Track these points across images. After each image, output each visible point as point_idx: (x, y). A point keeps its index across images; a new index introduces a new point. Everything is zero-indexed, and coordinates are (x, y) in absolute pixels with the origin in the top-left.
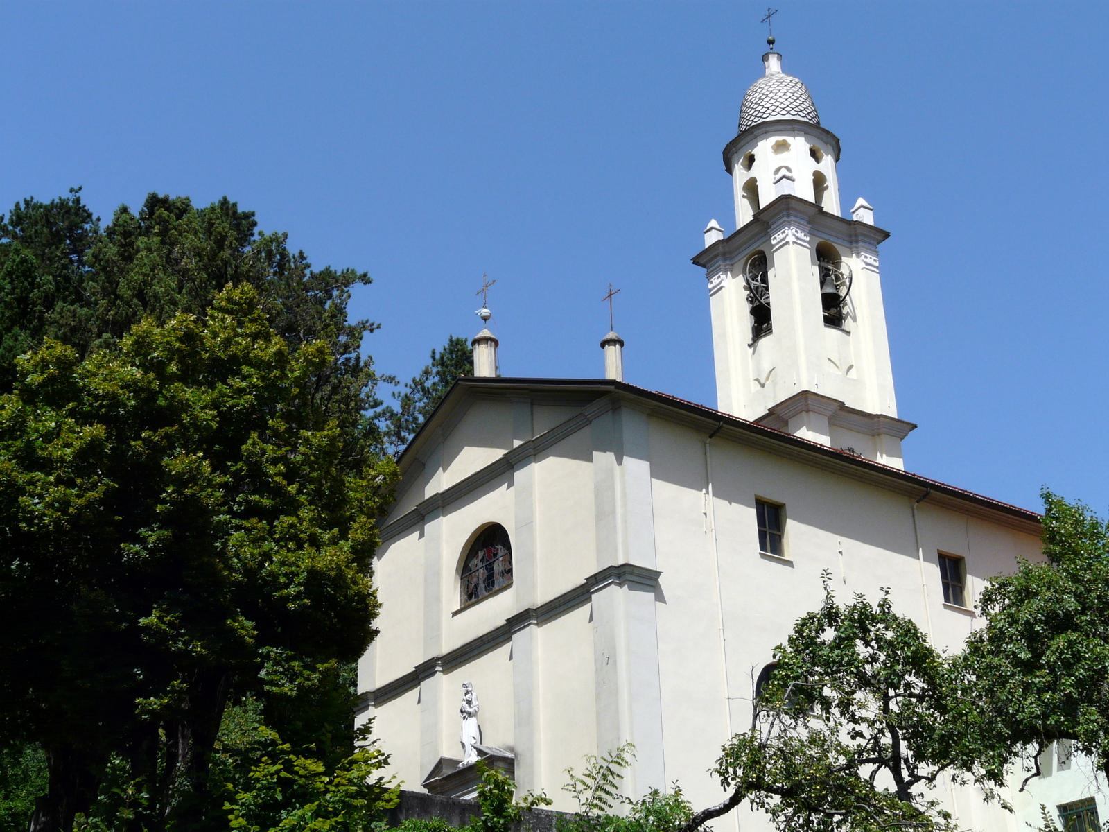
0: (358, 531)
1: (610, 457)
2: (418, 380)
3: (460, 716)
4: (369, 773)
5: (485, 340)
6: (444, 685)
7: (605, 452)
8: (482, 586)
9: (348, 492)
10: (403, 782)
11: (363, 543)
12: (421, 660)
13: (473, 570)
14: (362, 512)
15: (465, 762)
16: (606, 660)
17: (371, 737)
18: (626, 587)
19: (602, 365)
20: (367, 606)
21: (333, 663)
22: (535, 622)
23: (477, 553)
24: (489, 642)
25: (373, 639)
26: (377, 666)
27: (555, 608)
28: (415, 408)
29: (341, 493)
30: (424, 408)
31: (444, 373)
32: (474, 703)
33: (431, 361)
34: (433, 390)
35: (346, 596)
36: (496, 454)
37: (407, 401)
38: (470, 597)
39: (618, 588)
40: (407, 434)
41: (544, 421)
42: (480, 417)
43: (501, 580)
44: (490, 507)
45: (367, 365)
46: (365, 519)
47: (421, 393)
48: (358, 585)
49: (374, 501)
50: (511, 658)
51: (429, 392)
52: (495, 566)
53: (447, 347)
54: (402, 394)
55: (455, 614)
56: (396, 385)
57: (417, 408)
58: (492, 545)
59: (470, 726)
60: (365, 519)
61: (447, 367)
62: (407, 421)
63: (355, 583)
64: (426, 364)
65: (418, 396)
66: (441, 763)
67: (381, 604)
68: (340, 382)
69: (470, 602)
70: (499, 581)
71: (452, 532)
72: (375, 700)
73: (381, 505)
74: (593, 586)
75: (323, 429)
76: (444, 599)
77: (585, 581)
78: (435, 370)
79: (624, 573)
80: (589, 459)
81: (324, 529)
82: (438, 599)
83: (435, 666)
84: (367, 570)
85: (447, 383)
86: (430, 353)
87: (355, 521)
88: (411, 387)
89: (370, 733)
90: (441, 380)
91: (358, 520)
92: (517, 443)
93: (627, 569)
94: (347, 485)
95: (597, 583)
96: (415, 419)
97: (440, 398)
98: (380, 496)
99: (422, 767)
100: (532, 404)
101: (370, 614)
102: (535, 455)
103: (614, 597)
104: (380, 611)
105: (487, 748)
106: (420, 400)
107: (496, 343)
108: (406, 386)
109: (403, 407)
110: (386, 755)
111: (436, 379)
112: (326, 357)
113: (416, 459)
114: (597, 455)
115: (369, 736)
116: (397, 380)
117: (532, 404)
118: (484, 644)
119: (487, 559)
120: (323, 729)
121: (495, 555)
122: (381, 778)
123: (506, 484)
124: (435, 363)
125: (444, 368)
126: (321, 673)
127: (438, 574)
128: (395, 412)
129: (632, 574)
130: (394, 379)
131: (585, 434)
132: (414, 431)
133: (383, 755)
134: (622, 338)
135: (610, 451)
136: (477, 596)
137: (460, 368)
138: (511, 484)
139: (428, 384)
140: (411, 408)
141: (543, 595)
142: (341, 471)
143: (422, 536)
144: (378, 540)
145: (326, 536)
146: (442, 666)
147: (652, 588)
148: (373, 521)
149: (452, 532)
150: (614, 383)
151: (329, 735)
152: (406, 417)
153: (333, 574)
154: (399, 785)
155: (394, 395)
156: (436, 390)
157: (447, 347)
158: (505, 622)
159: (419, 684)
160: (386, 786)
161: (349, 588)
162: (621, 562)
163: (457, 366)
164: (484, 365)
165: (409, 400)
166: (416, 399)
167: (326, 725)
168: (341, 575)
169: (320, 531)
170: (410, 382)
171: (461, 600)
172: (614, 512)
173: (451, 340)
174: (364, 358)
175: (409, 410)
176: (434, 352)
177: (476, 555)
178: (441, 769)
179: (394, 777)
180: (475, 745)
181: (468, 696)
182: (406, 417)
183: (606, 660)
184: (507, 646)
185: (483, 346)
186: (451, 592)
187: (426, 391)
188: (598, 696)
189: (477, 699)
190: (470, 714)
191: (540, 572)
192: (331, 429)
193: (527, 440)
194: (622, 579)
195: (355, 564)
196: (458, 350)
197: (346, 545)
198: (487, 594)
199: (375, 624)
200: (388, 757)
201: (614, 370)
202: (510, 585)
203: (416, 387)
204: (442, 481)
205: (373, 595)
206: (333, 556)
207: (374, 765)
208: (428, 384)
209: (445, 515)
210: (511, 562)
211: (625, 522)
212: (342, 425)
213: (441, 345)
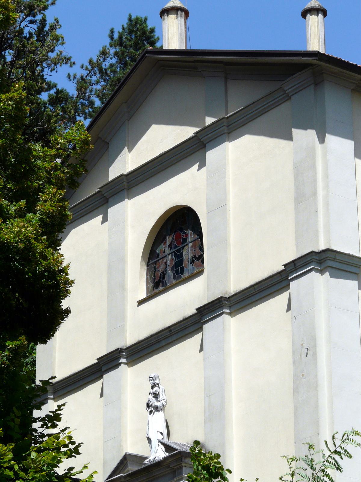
0: (46, 204)
1: (312, 134)
2: (95, 60)
3: (145, 410)
4: (60, 462)
5: (175, 10)
6: (129, 378)
7: (306, 129)
8: (170, 273)
9: (35, 161)
10: (96, 472)
11: (50, 216)
12: (104, 352)
13: (161, 256)
14: (50, 183)
15: (152, 458)
16: (305, 352)
17: (61, 425)
18: (327, 274)
19: (303, 36)
20: (58, 283)
21: (23, 340)
22: (228, 311)
23: (165, 238)
24: (177, 332)
25: (63, 319)
26: (57, 357)
27: (74, 383)
28: (91, 91)
29: (28, 163)
30: (101, 91)
31: (123, 53)
32: (162, 397)
33: (108, 41)
34: (111, 72)
35: (34, 272)
36: (187, 132)
37: (83, 84)
38: (157, 285)
39: (319, 275)
40: (82, 119)
41: (239, 98)
42: (168, 93)
43: (191, 266)
44: (179, 189)
45: (53, 28)
46: (55, 190)
47: (98, 75)
48: (48, 260)
49: (63, 172)
50: (201, 349)
51: (107, 74)
52: (184, 253)
53: (125, 26)
54: (78, 76)
55: (141, 303)
56: (71, 66)
57: (94, 90)
58: (181, 230)
59: (157, 422)
60: (55, 190)
61: (125, 47)
62: (82, 105)
63: (45, 258)
64: (104, 45)
65: (94, 78)
66: (126, 459)
67: (72, 281)
68: (24, 46)
69: (157, 291)
70: (189, 268)
71: (139, 215)
72: (54, 393)
73: (71, 176)
74: (292, 272)
75: (8, 91)
76: (129, 285)
77: (283, 268)
78: (112, 51)
79: (326, 259)
80: (289, 137)
81: (11, 200)
82: (123, 287)
83: (119, 358)
84: (55, 244)
85: (126, 64)
86: (108, 32)
87: (43, 193)
88: (87, 69)
89: (60, 420)
90: (120, 62)
91: (47, 191)
92: (209, 121)
93: (329, 254)
94: (35, 153)
95: (296, 270)
96: (92, 103)
97: (119, 80)
98: (70, 166)
99: (105, 463)
100: (226, 79)
101: (61, 291)
102: (229, 133)
103: (315, 285)
104: (72, 288)
105: (176, 443)
106: (98, 82)
107: (187, 14)
108: (82, 67)
109: (79, 89)
110: (77, 444)
111: (114, 61)
112: (11, 14)
113: (99, 137)
114: (296, 133)
115: (58, 423)
116: (72, 60)
117: (226, 79)
118: (172, 335)
119: (176, 245)
120: (12, 415)
121: (185, 240)
122: (72, 469)
123: (197, 165)
124: (113, 43)
125: (123, 49)
126: (10, 350)
127: (123, 260)
128: (71, 94)
129: (334, 260)
130: (69, 59)
131: (284, 109)
132: (90, 116)
133: (73, 443)
134: (325, 7)
135: (312, 128)
136: (164, 284)
137: (140, 49)
138: (203, 165)
139: (106, 65)
140: (88, 91)
141: (235, 284)
142: (26, 141)
143: (105, 220)
144: (68, 213)
145: (13, 209)
146: (126, 358)
147: (354, 276)
148: (63, 192)
149: (139, 215)
150: (316, 54)
151: (18, 421)
152: (82, 101)
153: (21, 246)
154: (91, 476)
155: (69, 77)
156: (114, 72)
157: (125, 26)
158: (195, 311)
159: (101, 377)
160: (77, 477)
161: (37, 263)
162: (322, 247)
163: (137, 47)
164: (172, 36)
165: (85, 82)
166: (93, 82)
167: (15, 409)
168: (29, 248)
169: (6, 202)
170: (87, 64)
171: (147, 288)
172: (315, 194)
173: (130, 19)
174: (50, 21)
175: (85, 93)
176: (112, 32)
177: (164, 240)
178: (126, 466)
179: (86, 467)
180: (163, 441)
181: (155, 389)
182: (82, 101)
183: (305, 352)
184: (197, 338)
185: (172, 16)
186: (136, 278)
187: (103, 73)
188: (296, 390)
189: (164, 393)
190: (157, 409)
191: (235, 256)
192: (16, 91)
193: (222, 117)
194: (324, 266)
195: (45, 237)
196: (138, 30)
197: (34, 218)
198: (175, 282)
199: (65, 304)
200: (79, 446)
201: (317, 41)
202: (201, 272)
203: (93, 68)
204: (127, 162)
205: (65, 271)
206: (21, 228)
207: (65, 453)
208: (106, 65)
209: (130, 198)
210: (201, 248)
211: (327, 204)
212: (27, 89)
213: (119, 24)
